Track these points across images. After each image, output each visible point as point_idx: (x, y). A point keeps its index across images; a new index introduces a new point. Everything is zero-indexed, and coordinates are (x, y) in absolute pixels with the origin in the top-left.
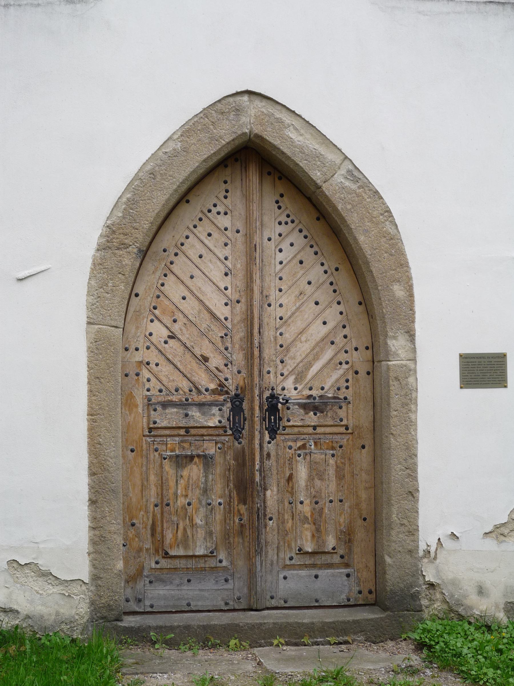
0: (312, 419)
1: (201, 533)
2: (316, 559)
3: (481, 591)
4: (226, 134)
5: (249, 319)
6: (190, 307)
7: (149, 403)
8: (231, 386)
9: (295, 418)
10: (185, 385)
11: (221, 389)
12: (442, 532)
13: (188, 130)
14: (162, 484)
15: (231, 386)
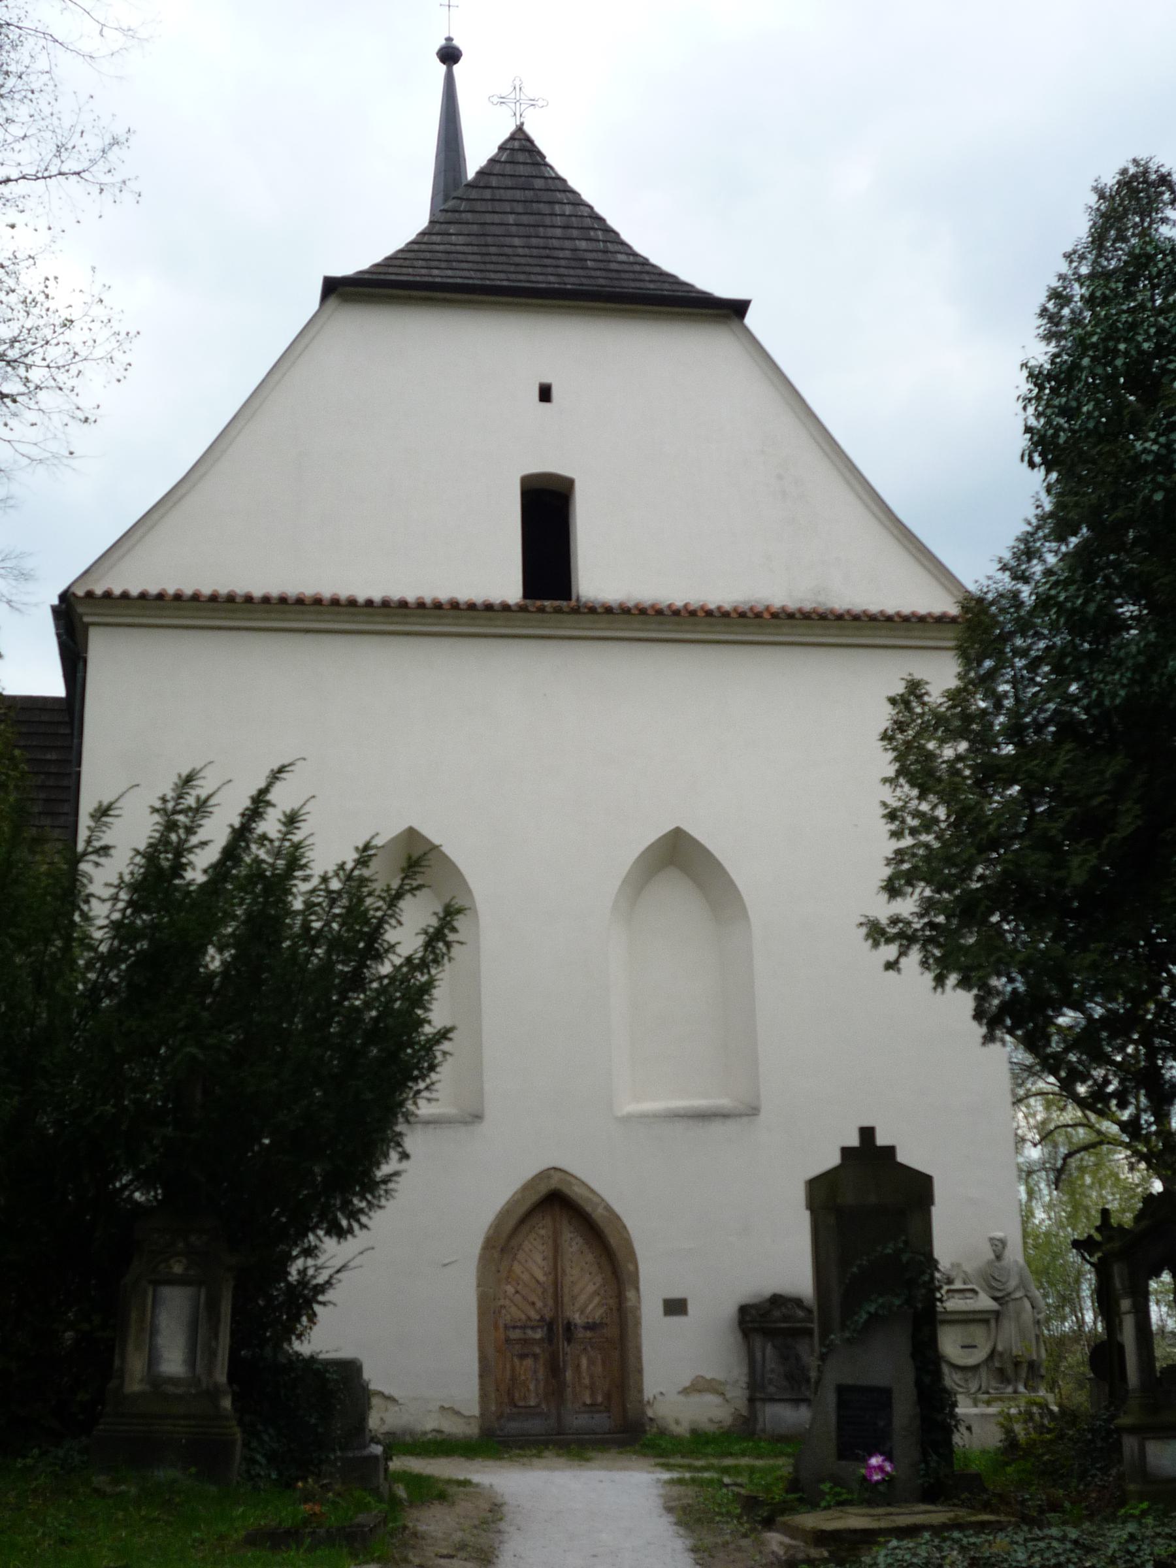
0: (589, 1334)
1: (533, 1395)
2: (592, 1408)
3: (677, 1422)
4: (543, 1189)
5: (556, 1283)
6: (525, 1277)
7: (506, 1327)
8: (547, 1317)
9: (580, 1334)
10: (523, 1317)
11: (542, 1319)
12: (656, 1391)
13: (526, 1188)
14: (513, 1369)
15: (547, 1317)
